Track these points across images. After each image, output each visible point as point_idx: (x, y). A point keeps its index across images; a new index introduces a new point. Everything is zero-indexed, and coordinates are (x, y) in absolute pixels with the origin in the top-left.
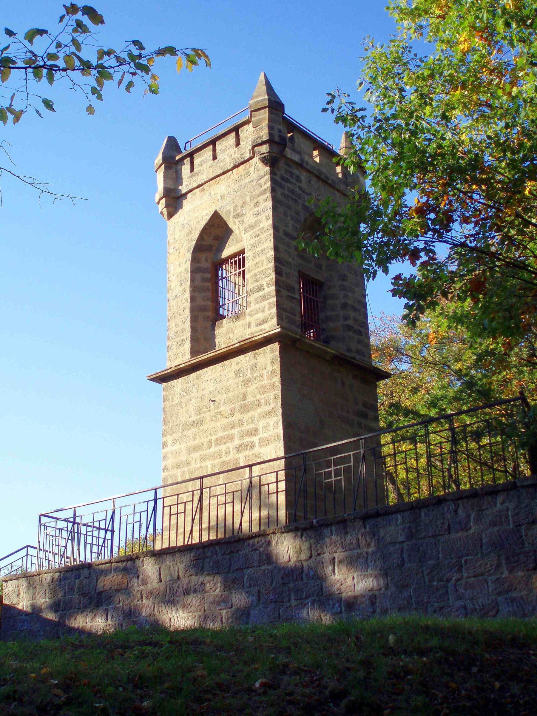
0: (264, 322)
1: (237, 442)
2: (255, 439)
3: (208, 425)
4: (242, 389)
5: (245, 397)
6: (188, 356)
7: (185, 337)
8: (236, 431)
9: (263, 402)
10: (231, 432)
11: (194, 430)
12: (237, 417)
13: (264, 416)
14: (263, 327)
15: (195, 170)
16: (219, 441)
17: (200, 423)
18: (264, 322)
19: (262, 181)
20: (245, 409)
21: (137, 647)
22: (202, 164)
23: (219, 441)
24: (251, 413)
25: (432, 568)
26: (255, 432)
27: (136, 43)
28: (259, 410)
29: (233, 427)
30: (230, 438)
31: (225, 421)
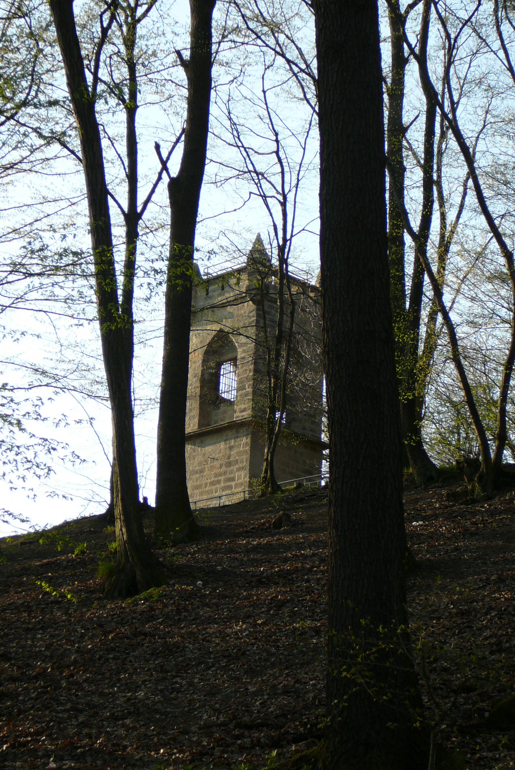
0: (244, 410)
1: (222, 484)
2: (233, 483)
3: (206, 472)
4: (228, 451)
5: (229, 457)
6: (196, 427)
7: (195, 413)
8: (222, 478)
9: (239, 461)
10: (219, 478)
11: (197, 475)
12: (224, 468)
13: (239, 469)
14: (244, 413)
15: (210, 294)
16: (212, 483)
17: (202, 471)
18: (244, 410)
19: (251, 314)
20: (229, 464)
21: (62, 265)
22: (214, 291)
23: (212, 483)
24: (232, 468)
25: (17, 299)
26: (233, 479)
27: (57, 425)
28: (237, 466)
29: (221, 475)
30: (219, 482)
31: (215, 471)
